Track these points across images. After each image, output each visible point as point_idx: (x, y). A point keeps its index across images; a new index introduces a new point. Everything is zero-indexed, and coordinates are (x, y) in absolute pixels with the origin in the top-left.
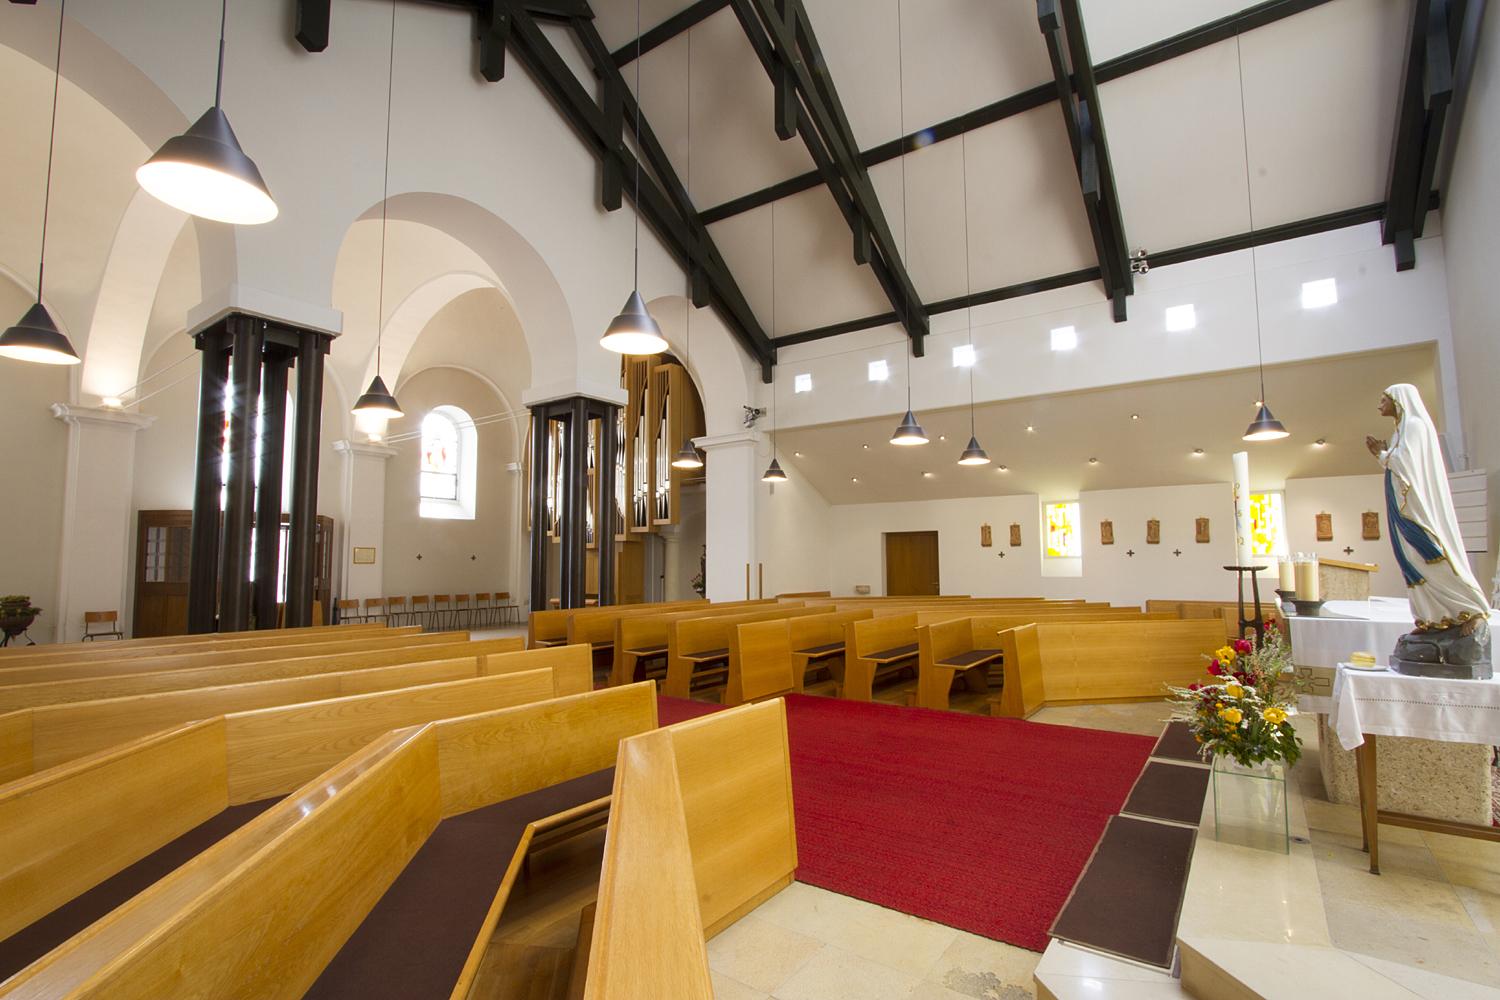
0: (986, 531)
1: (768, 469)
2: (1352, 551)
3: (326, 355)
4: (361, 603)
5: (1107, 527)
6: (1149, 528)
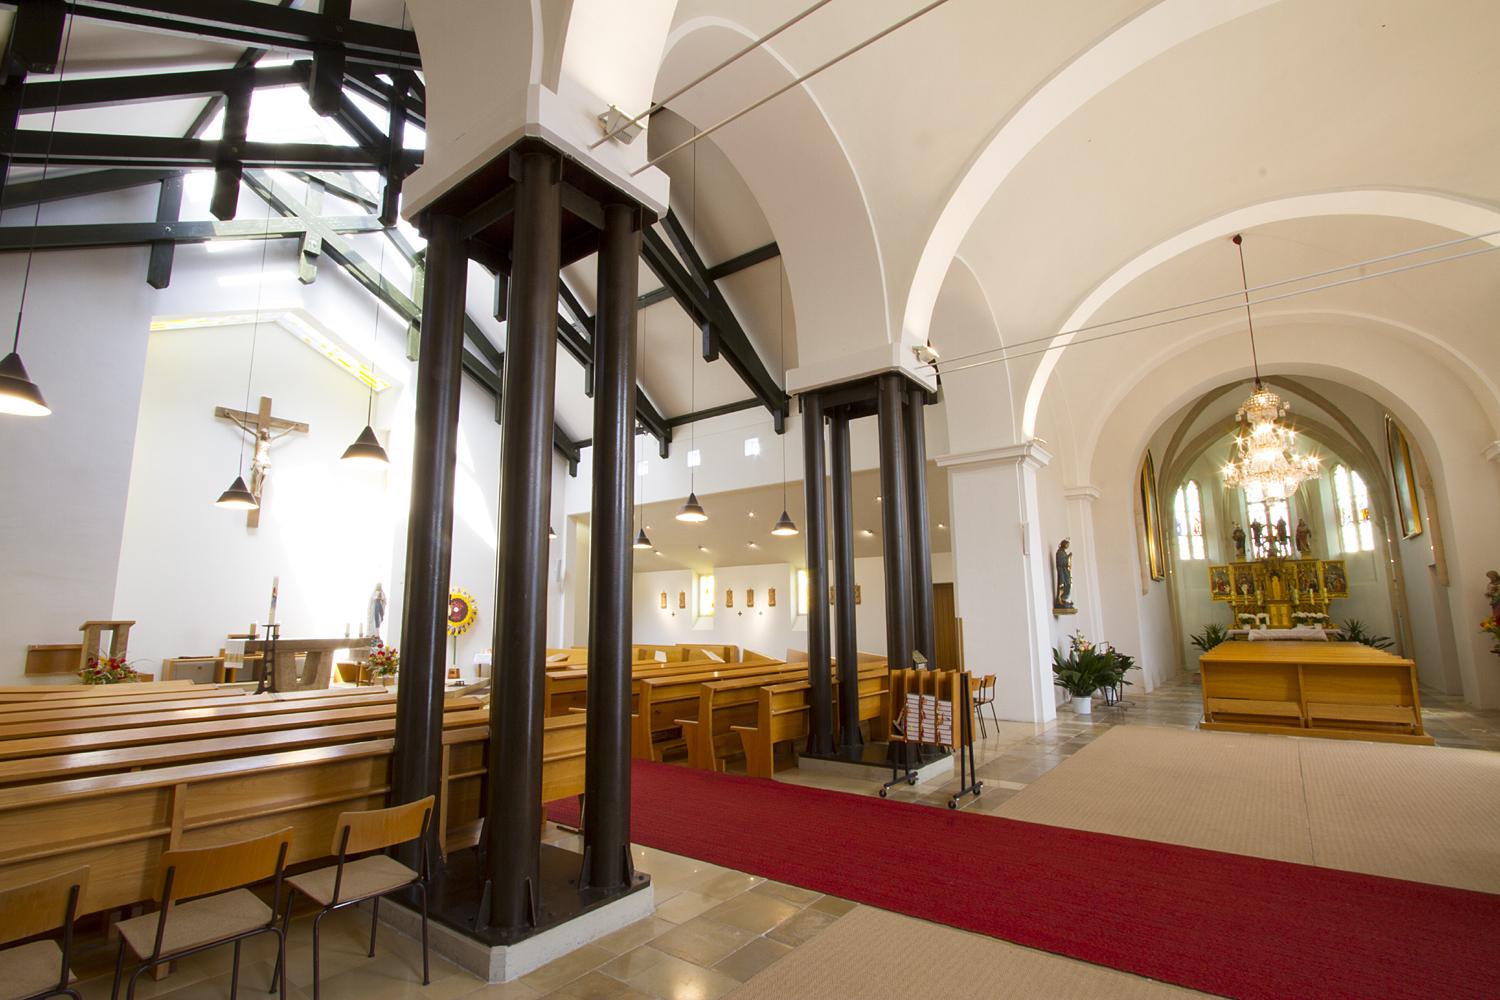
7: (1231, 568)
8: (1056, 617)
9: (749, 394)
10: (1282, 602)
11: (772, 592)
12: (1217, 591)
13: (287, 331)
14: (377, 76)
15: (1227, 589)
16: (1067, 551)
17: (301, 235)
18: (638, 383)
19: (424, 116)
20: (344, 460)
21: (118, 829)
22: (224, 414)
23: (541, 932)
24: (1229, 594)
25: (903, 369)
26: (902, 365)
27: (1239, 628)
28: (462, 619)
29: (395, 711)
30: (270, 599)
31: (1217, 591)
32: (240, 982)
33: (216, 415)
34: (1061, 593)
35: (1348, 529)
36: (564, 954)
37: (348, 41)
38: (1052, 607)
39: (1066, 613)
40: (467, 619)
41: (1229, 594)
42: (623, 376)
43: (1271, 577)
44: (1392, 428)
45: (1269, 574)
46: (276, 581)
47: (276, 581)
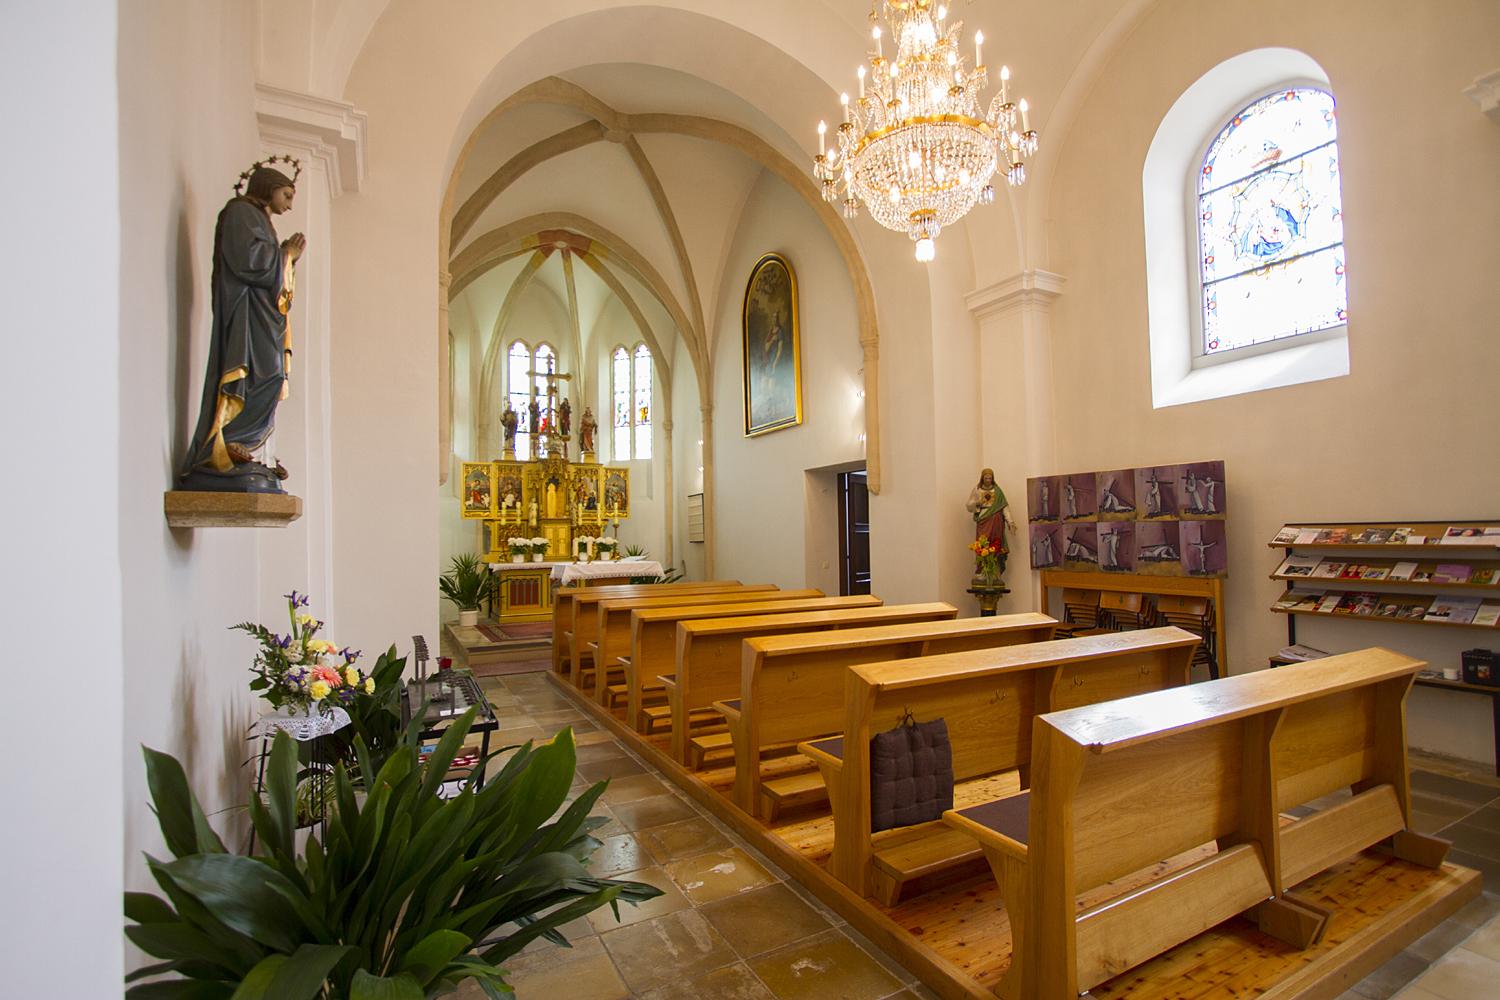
7: (494, 469)
8: (181, 537)
10: (557, 521)
12: (471, 502)
15: (486, 500)
16: (283, 226)
19: (386, 976)
20: (141, 752)
24: (487, 509)
27: (507, 561)
31: (471, 502)
34: (226, 413)
35: (622, 434)
37: (176, 983)
38: (160, 481)
39: (250, 516)
41: (487, 509)
43: (547, 484)
44: (751, 303)
45: (546, 480)
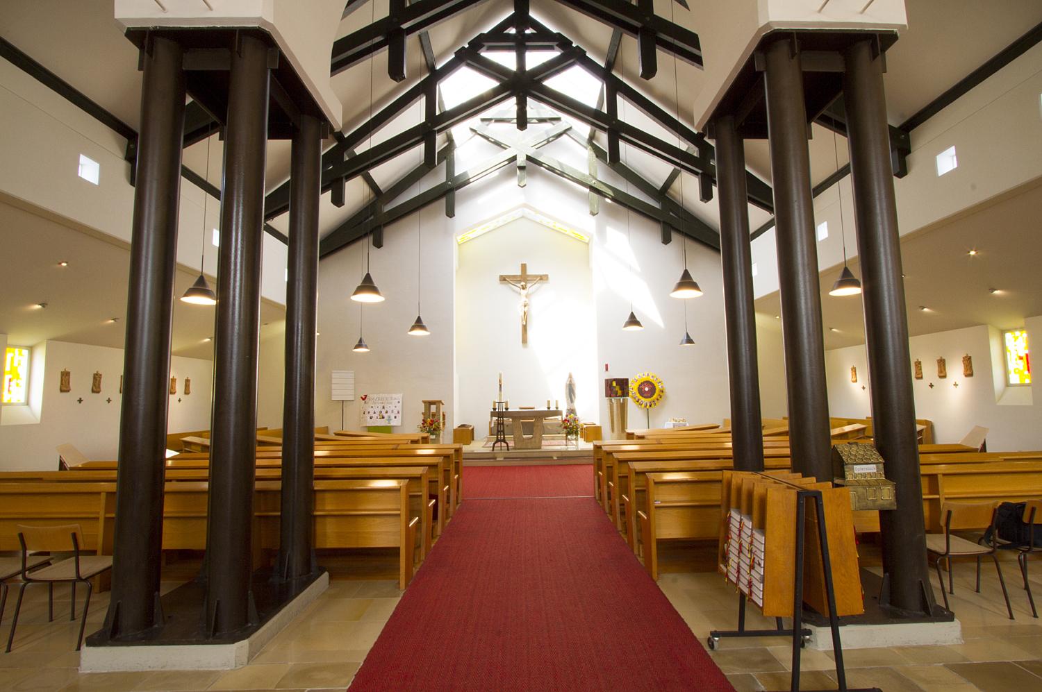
0: (97, 378)
1: (191, 287)
2: (80, 399)
3: (809, 141)
4: (633, 387)
5: (65, 375)
6: (95, 378)
9: (185, 186)
11: (968, 361)
13: (529, 219)
14: (505, 32)
17: (514, 159)
18: (747, 168)
21: (394, 507)
22: (503, 279)
23: (146, 645)
25: (778, 23)
26: (772, 19)
28: (651, 396)
29: (281, 464)
30: (499, 386)
32: (47, 608)
33: (500, 280)
36: (133, 670)
40: (655, 396)
42: (238, 202)
46: (500, 375)
47: (500, 375)
